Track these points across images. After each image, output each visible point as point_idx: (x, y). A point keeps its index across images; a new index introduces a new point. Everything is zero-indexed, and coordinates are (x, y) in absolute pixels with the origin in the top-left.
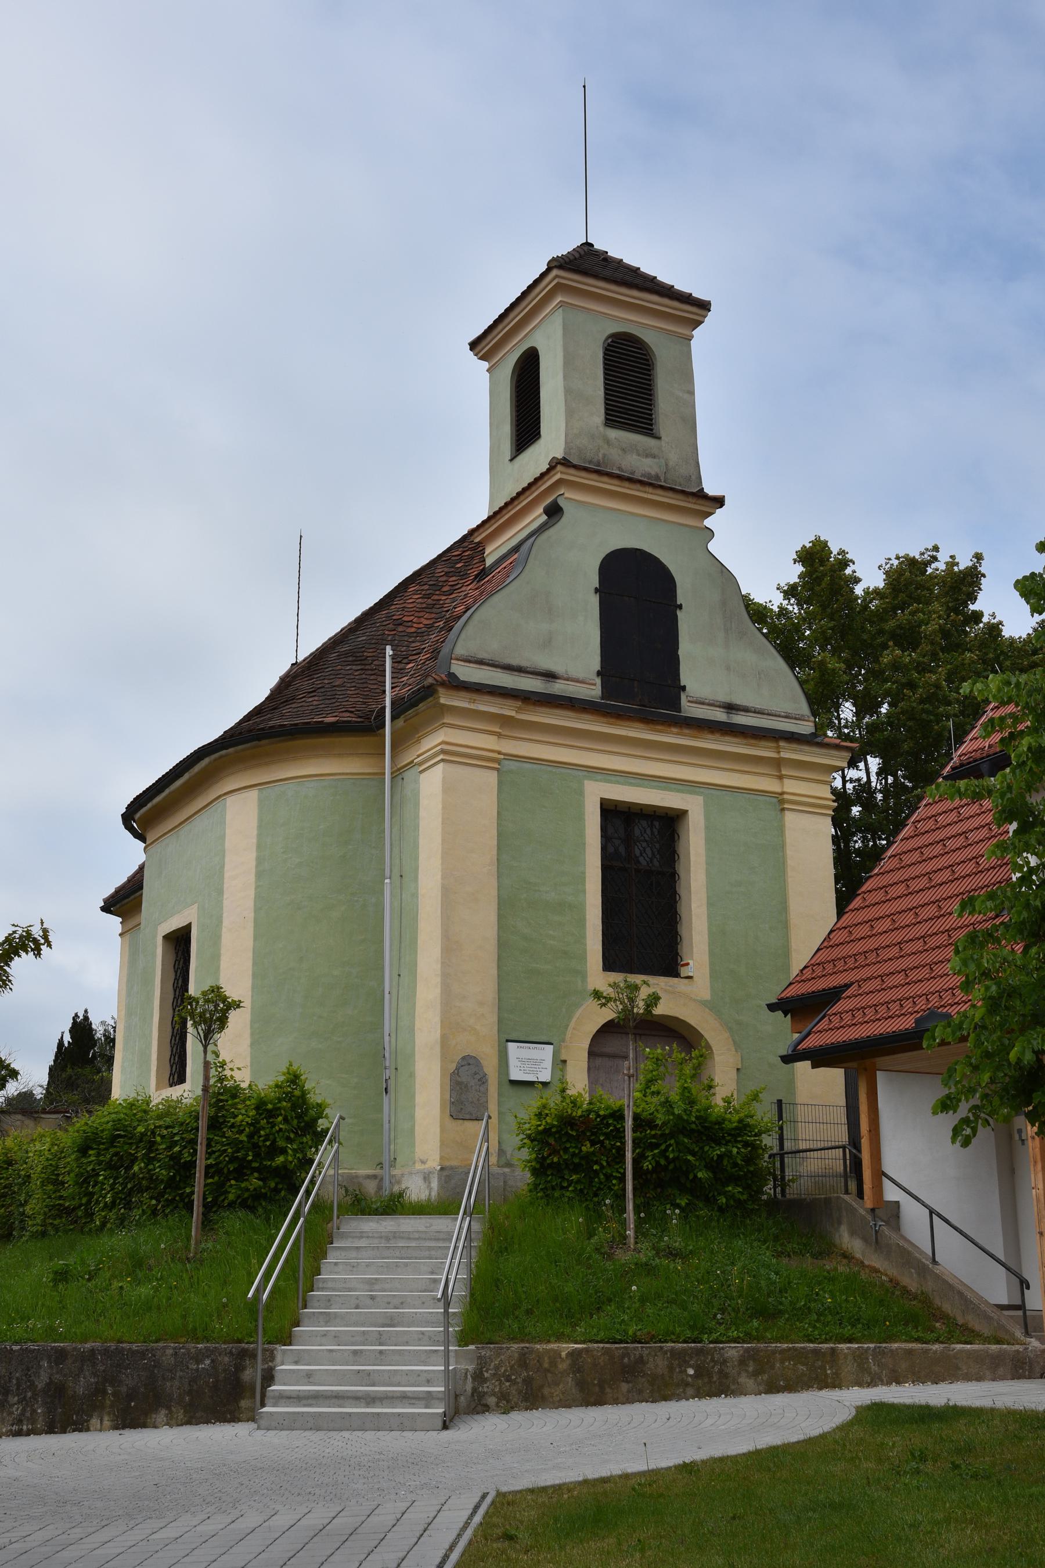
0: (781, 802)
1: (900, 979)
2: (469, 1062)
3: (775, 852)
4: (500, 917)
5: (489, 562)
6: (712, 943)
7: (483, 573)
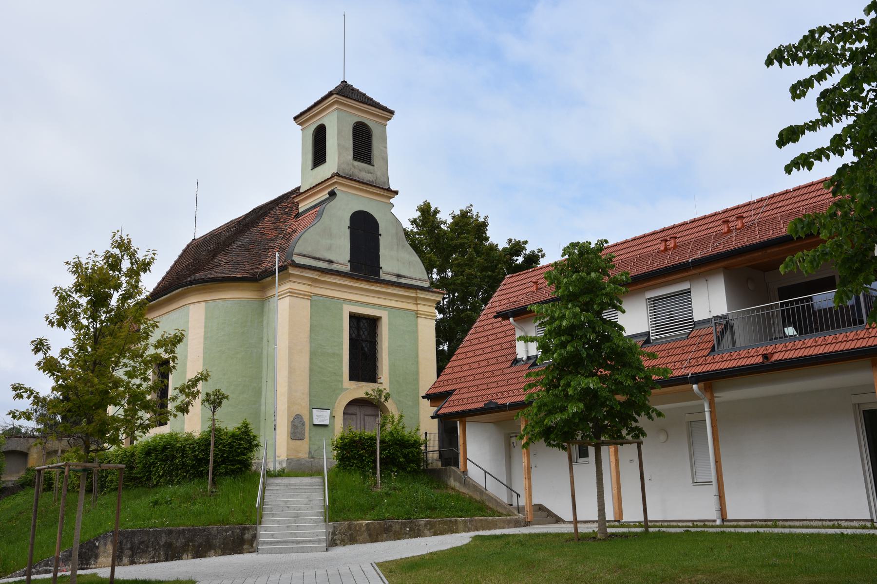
0: (417, 314)
1: (475, 388)
2: (298, 417)
3: (414, 333)
4: (311, 359)
5: (300, 211)
6: (390, 370)
7: (298, 215)
